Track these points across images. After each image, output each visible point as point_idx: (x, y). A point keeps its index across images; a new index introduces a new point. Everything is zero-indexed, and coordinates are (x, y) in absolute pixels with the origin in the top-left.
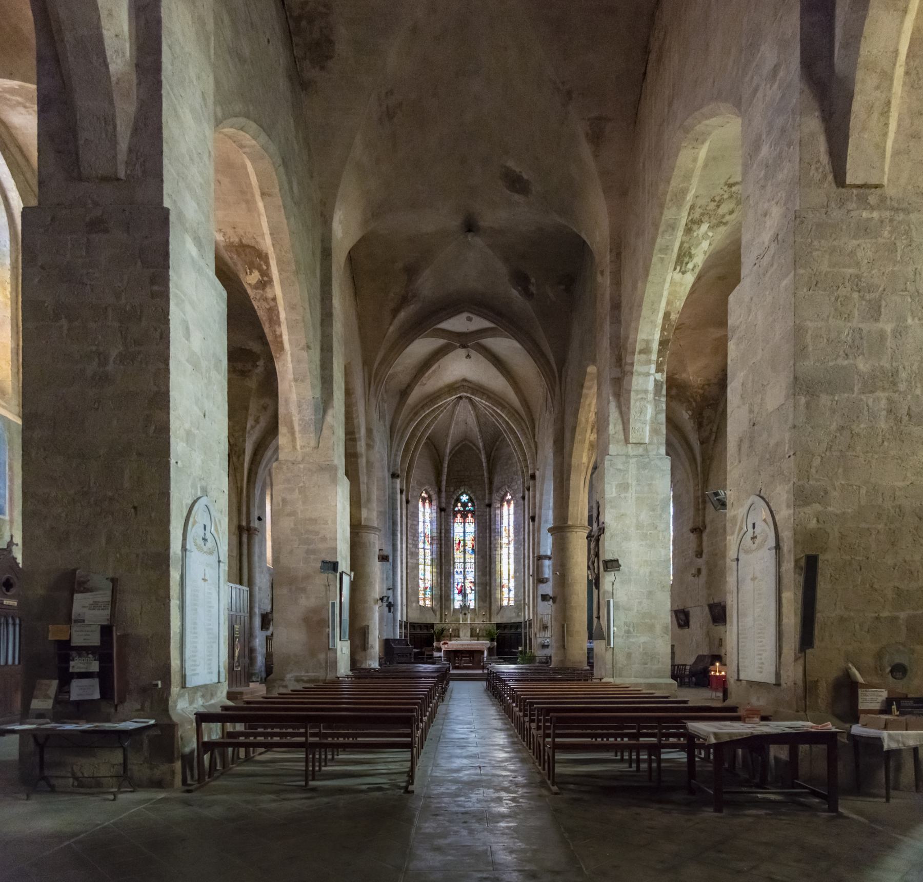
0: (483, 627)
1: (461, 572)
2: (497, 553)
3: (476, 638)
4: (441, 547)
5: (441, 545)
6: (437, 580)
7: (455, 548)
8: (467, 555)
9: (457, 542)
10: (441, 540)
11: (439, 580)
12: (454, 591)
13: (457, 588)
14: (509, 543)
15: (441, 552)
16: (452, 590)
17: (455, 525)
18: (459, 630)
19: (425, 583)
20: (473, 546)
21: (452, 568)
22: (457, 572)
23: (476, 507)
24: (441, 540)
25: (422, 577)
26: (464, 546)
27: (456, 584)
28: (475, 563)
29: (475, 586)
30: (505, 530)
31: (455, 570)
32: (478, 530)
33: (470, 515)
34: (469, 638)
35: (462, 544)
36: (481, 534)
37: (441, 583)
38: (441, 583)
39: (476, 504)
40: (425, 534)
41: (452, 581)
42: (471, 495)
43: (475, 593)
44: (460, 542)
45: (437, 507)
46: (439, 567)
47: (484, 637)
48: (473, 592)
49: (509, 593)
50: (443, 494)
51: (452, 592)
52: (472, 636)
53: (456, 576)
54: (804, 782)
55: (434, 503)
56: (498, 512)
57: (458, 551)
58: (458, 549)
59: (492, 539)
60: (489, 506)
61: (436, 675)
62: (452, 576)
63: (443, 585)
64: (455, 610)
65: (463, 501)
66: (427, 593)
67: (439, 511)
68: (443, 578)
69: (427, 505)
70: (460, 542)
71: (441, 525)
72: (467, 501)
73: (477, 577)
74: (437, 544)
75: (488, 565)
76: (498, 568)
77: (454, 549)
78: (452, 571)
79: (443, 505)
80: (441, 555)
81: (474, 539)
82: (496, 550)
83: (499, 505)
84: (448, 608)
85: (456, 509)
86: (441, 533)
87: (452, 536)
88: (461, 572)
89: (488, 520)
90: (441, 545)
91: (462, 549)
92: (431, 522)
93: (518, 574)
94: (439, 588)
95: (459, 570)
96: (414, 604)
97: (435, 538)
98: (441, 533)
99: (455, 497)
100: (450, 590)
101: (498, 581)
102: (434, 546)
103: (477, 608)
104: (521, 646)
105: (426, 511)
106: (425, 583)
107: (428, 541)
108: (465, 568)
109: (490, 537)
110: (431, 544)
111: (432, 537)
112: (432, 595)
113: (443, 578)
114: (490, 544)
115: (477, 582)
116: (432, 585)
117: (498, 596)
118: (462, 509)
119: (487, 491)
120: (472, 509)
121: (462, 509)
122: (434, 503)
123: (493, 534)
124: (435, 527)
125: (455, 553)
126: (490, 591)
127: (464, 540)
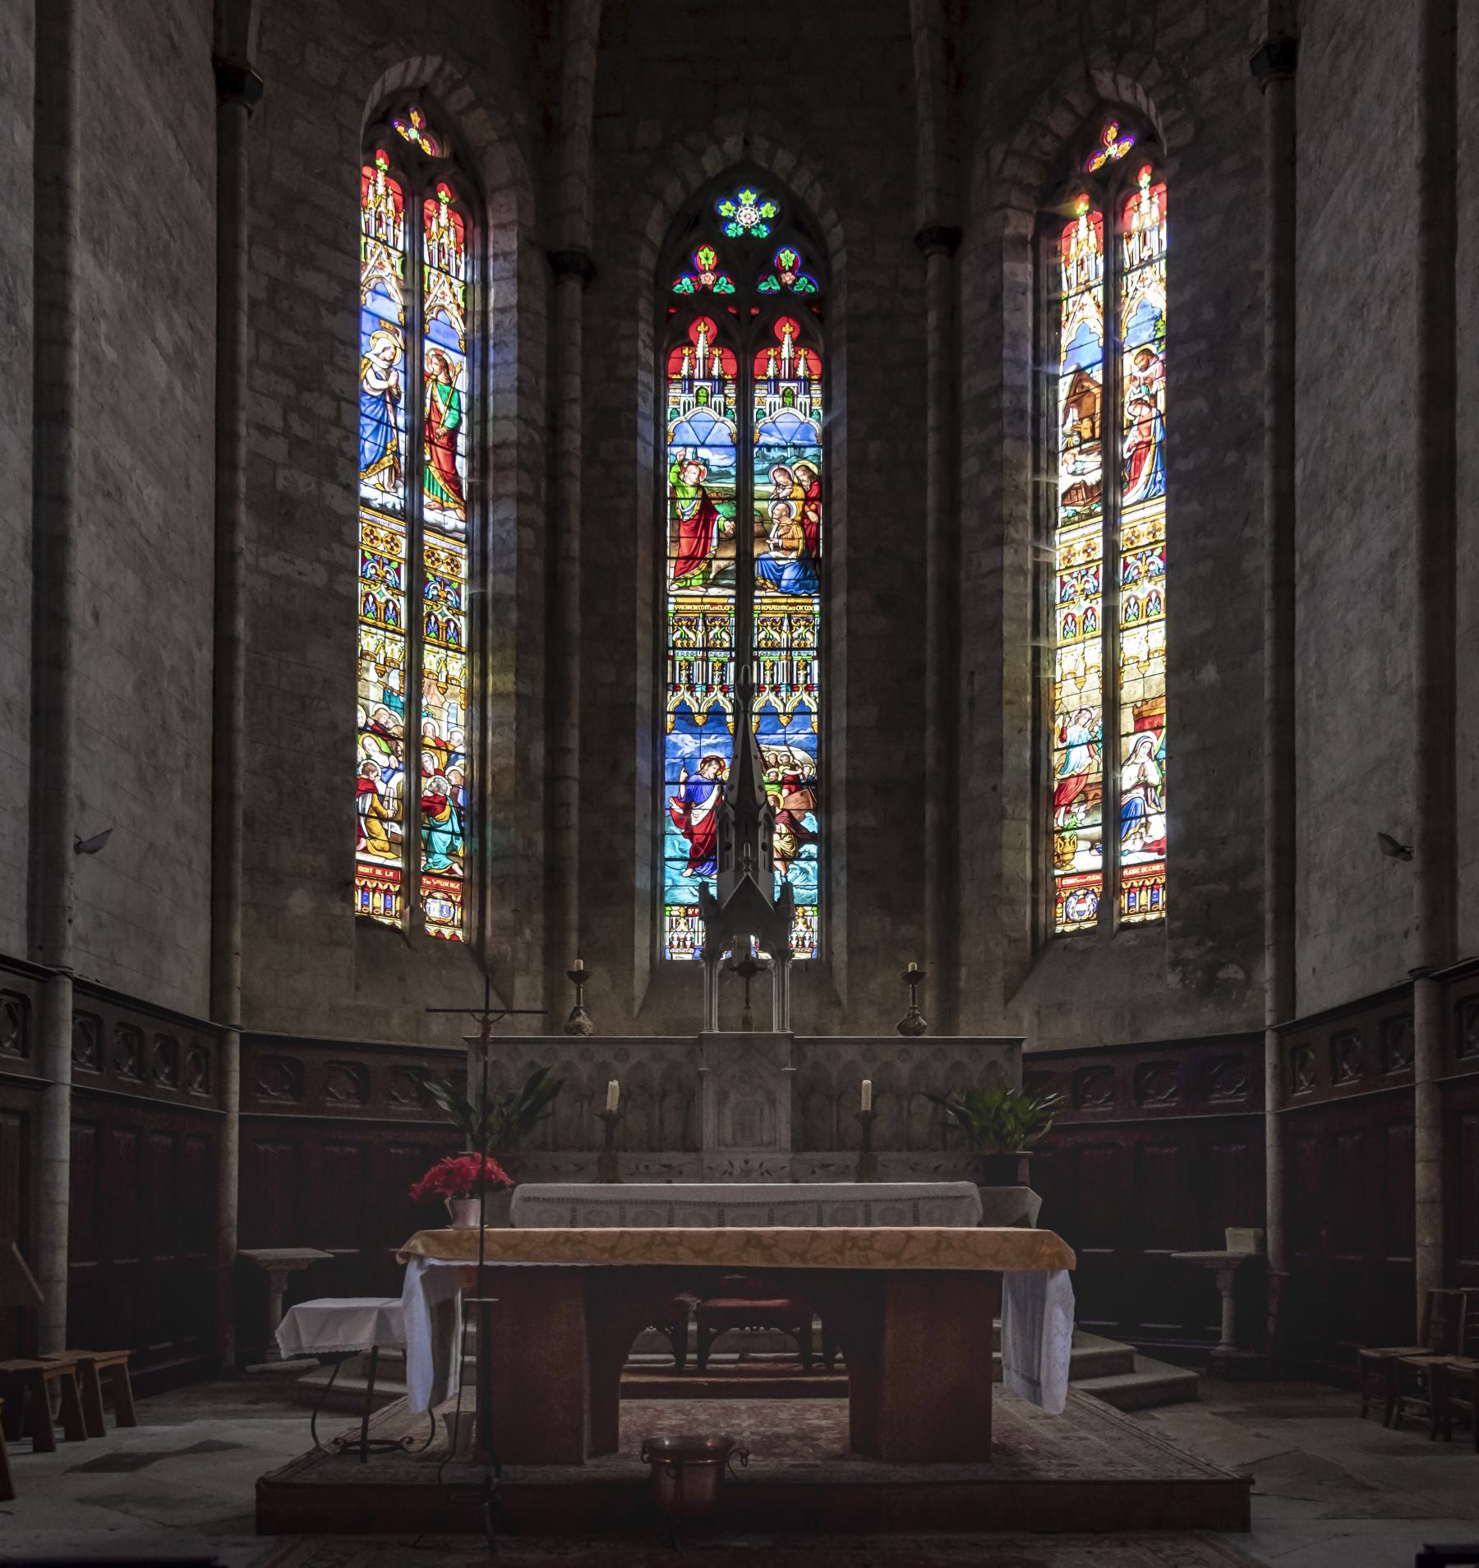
0: (904, 1069)
1: (716, 713)
2: (1009, 558)
3: (852, 1158)
4: (554, 529)
5: (555, 509)
6: (522, 757)
7: (672, 551)
8: (767, 602)
9: (688, 507)
10: (555, 476)
11: (538, 751)
12: (658, 842)
13: (683, 821)
14: (1116, 475)
15: (554, 560)
16: (643, 825)
17: (676, 395)
18: (689, 1099)
19: (415, 770)
20: (810, 541)
21: (643, 679)
22: (683, 713)
23: (839, 262)
24: (555, 476)
25: (394, 722)
26: (748, 531)
27: (673, 794)
28: (824, 652)
29: (821, 808)
30: (1078, 395)
31: (672, 702)
32: (852, 414)
33: (787, 331)
34: (783, 1158)
35: (724, 522)
36: (874, 448)
37: (554, 777)
38: (554, 777)
39: (836, 237)
40: (420, 430)
41: (643, 767)
42: (798, 186)
43: (825, 860)
44: (707, 511)
45: (527, 244)
46: (538, 663)
47: (909, 1144)
48: (812, 849)
49: (1109, 844)
50: (579, 155)
51: (642, 844)
52: (804, 1140)
53: (685, 743)
54: (979, 1225)
55: (502, 209)
56: (1019, 271)
57: (696, 576)
58: (690, 560)
59: (970, 467)
60: (949, 239)
61: (1126, 633)
62: (643, 735)
63: (574, 792)
64: (665, 973)
65: (732, 231)
66: (440, 840)
67: (538, 268)
68: (574, 741)
69: (442, 222)
70: (707, 511)
71: (555, 371)
72: (764, 232)
73: (840, 745)
74: (521, 499)
75: (930, 653)
76: (1017, 667)
77: (660, 559)
78: (643, 700)
79: (579, 232)
80: (554, 581)
81: (821, 491)
82: (1000, 541)
83: (1025, 226)
84: (616, 953)
85: (685, 285)
86: (554, 428)
87: (645, 457)
88: (716, 713)
89: (932, 343)
90: (555, 509)
91: (724, 558)
92: (477, 349)
93: (1209, 674)
94: (537, 807)
95: (698, 703)
96: (300, 902)
97: (510, 455)
98: (554, 428)
99: (674, 193)
100: (630, 831)
101: (1019, 756)
102: (501, 514)
103: (840, 957)
104: (1256, 1219)
105: (429, 249)
106: (415, 770)
107: (453, 480)
108: (745, 691)
109: (952, 455)
110: (476, 502)
111: (480, 455)
112: (477, 861)
113: (574, 741)
114: (951, 505)
115: (840, 772)
116: (476, 786)
117: (1018, 864)
118: (725, 287)
119: (927, 133)
120: (804, 285)
121: (725, 287)
122: (502, 209)
123: (971, 438)
124: (504, 375)
125: (673, 588)
126: (949, 832)
127: (743, 497)
